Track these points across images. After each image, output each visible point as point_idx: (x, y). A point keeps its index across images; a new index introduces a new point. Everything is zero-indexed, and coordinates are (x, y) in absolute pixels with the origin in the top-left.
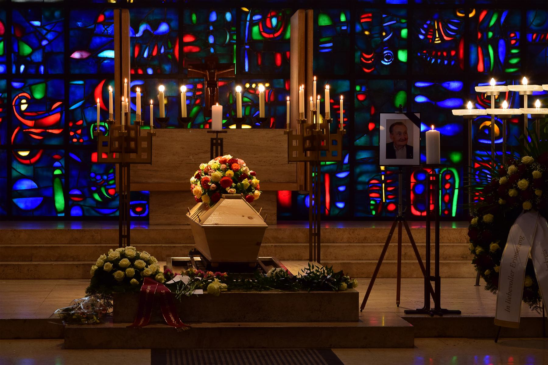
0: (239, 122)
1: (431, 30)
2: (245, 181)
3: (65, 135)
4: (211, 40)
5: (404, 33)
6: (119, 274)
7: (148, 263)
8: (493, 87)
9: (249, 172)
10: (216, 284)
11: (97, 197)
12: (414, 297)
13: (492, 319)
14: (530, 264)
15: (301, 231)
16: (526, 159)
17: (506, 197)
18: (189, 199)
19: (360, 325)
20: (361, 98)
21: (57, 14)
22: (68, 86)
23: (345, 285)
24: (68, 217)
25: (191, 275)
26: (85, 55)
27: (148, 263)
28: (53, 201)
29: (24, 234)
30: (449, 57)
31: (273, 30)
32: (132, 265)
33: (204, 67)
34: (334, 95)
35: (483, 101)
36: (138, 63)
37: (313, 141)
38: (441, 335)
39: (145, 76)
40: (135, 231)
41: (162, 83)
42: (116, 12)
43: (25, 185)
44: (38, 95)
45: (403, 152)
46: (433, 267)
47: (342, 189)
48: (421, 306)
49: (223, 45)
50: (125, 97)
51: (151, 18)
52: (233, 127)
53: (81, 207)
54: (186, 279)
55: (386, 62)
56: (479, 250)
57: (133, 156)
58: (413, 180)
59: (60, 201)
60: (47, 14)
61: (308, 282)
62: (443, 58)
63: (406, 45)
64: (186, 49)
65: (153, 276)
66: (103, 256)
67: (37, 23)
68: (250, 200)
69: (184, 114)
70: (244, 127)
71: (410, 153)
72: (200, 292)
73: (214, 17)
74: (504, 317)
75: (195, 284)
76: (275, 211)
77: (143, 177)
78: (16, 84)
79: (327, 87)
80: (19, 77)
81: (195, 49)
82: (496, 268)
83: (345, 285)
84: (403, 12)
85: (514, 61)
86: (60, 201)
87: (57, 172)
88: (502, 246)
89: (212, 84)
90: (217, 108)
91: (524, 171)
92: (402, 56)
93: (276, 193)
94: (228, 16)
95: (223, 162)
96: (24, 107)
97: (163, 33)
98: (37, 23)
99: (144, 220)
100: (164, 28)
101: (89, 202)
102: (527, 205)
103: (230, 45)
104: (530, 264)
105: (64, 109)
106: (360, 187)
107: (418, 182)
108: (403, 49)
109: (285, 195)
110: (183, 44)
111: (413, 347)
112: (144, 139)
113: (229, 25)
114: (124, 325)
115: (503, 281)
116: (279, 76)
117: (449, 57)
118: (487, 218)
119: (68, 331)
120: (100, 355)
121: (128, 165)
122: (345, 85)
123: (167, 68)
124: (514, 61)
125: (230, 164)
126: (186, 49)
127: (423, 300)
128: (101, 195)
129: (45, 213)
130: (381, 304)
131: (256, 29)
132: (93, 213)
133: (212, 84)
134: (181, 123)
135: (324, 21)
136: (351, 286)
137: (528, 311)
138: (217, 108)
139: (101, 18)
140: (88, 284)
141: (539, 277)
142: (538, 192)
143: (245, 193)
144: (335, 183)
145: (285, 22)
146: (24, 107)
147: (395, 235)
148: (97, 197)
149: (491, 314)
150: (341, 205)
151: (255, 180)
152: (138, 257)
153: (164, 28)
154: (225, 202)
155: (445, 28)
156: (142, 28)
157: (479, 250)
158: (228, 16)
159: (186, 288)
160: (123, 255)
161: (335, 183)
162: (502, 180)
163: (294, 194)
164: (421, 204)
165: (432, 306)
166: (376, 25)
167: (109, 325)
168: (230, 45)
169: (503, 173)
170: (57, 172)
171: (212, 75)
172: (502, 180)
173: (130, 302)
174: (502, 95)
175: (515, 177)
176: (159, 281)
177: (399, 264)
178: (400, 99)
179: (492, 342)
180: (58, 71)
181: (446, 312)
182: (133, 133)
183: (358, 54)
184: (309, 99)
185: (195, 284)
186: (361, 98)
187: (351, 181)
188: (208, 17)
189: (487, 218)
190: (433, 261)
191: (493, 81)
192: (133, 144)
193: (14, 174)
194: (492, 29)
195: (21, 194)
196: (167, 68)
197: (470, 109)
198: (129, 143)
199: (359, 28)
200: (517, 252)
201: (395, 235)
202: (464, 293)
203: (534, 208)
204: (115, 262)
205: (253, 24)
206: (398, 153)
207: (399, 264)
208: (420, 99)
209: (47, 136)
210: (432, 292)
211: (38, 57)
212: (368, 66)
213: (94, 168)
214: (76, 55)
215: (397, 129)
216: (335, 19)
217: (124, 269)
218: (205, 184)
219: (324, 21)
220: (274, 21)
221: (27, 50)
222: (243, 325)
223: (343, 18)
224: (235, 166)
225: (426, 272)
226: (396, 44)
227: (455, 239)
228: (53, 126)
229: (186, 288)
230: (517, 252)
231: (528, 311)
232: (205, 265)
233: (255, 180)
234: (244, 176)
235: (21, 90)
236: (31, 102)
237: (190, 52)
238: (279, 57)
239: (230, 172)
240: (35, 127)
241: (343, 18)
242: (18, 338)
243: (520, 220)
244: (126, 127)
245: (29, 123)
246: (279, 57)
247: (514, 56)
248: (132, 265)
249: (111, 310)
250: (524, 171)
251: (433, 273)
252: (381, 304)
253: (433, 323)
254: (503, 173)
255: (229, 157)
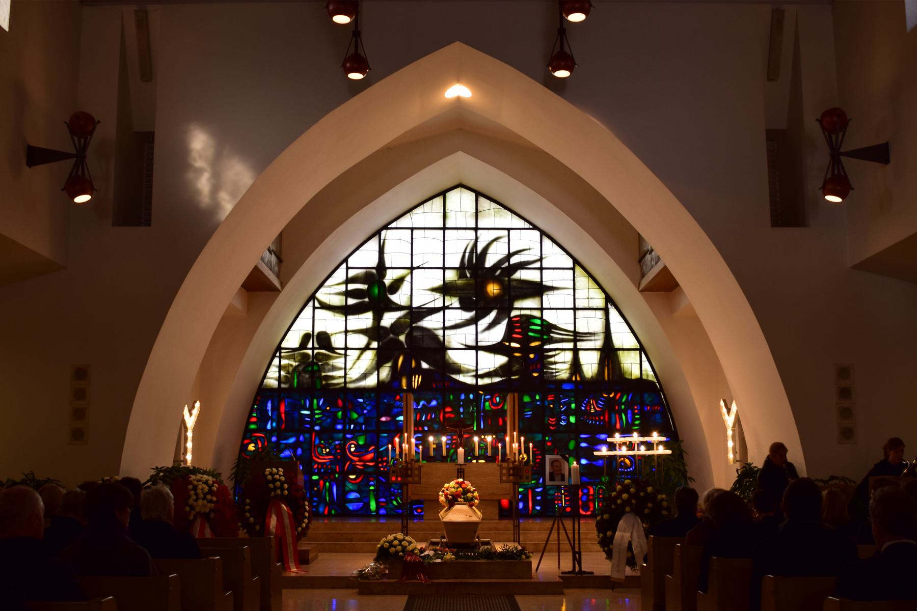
0: (478, 458)
1: (588, 404)
2: (469, 495)
3: (376, 466)
4: (461, 410)
5: (573, 406)
6: (392, 550)
7: (410, 543)
8: (617, 438)
9: (473, 489)
10: (449, 556)
11: (395, 503)
12: (567, 564)
13: (609, 577)
14: (630, 543)
15: (508, 524)
16: (627, 481)
17: (616, 504)
18: (440, 506)
19: (532, 580)
20: (549, 444)
21: (373, 395)
22: (378, 437)
23: (524, 557)
24: (378, 515)
25: (435, 550)
26: (389, 419)
27: (410, 543)
28: (369, 506)
29: (351, 525)
30: (600, 421)
31: (498, 404)
32: (400, 544)
33: (456, 426)
34: (526, 442)
35: (612, 447)
36: (418, 424)
37: (517, 472)
38: (582, 587)
39: (423, 431)
40: (412, 524)
41: (432, 435)
42: (404, 394)
43: (353, 496)
44: (361, 443)
45: (558, 477)
46: (577, 546)
47: (539, 498)
48: (571, 569)
49: (468, 413)
50: (408, 444)
51: (427, 397)
52: (474, 461)
53: (385, 509)
54: (431, 553)
55: (563, 423)
56: (601, 535)
57: (410, 479)
58: (580, 493)
59: (373, 506)
60: (367, 395)
61: (505, 555)
62: (596, 421)
63: (575, 413)
64: (447, 415)
65: (412, 551)
66: (384, 539)
67: (361, 400)
68: (471, 506)
69: (444, 453)
70: (480, 461)
71: (563, 479)
72: (439, 561)
73: (463, 397)
74: (616, 576)
75: (437, 556)
76: (497, 511)
77: (414, 491)
78: (348, 436)
79: (522, 439)
80: (350, 431)
81: (452, 416)
82: (611, 546)
83: (524, 557)
84: (572, 394)
85: (637, 422)
86: (373, 506)
87: (372, 488)
88: (614, 533)
89: (461, 436)
90: (461, 450)
91: (626, 489)
92: (572, 419)
93: (499, 502)
94: (471, 396)
95: (457, 483)
96: (353, 449)
97: (434, 406)
98: (361, 400)
99: (420, 517)
100: (434, 403)
101: (390, 506)
102: (627, 509)
103: (473, 413)
104: (630, 543)
105: (376, 451)
106: (549, 497)
107: (584, 494)
108: (572, 415)
109: (505, 502)
110: (445, 413)
111: (563, 594)
112: (416, 469)
113: (472, 401)
114: (393, 581)
115: (615, 555)
116: (500, 432)
117: (600, 421)
118: (606, 516)
119: (362, 585)
120: (378, 598)
121: (407, 484)
122: (539, 437)
123: (436, 426)
124: (637, 422)
125: (460, 484)
126: (447, 415)
127: (571, 565)
128: (397, 502)
129: (364, 512)
130: (547, 567)
131: (487, 404)
132: (393, 513)
133: (461, 436)
134: (444, 459)
135: (527, 399)
136: (528, 557)
137: (628, 571)
138: (461, 450)
139: (398, 397)
140: (375, 555)
141: (635, 552)
142: (633, 501)
143: (469, 502)
144: (535, 494)
145: (503, 400)
146: (353, 449)
147: (556, 526)
148: (395, 503)
149: (608, 574)
150: (538, 508)
151: (476, 494)
152: (404, 540)
153: (434, 403)
154: (457, 507)
155: (597, 403)
156: (422, 403)
157: (601, 535)
158: (471, 396)
159: (431, 558)
160: (395, 539)
161: (535, 494)
162: (614, 494)
163: (510, 502)
164: (586, 508)
165: (577, 569)
166: (557, 401)
167: (385, 580)
168: (473, 413)
169: (614, 490)
170: (372, 488)
171: (461, 431)
172: (614, 494)
173: (399, 569)
174: (642, 443)
175: (620, 493)
176: (416, 554)
177: (559, 544)
178: (572, 445)
179: (610, 591)
180: (373, 428)
181: (585, 572)
182: (409, 466)
183: (546, 418)
184: (514, 443)
185: (437, 556)
186: (549, 444)
187: (544, 493)
188: (460, 396)
189: (606, 516)
190: (577, 542)
191: (635, 434)
192: (409, 472)
193: (347, 489)
194: (624, 403)
195: (351, 501)
196: (436, 426)
197: (604, 451)
198: (408, 469)
199: (546, 403)
200: (622, 537)
201: (556, 526)
202: (596, 562)
203: (632, 510)
204: (391, 543)
205: (485, 400)
206: (556, 478)
207: (559, 544)
208: (583, 445)
209: (365, 466)
210: (577, 560)
211: (361, 420)
212: (552, 425)
213: (393, 486)
214: (383, 419)
215: (556, 464)
216: (533, 398)
217: (395, 547)
218: (446, 496)
219: (527, 399)
220: (498, 399)
221: (355, 416)
222: (463, 581)
223: (537, 398)
224: (463, 485)
225: (573, 548)
226: (569, 412)
227: (589, 529)
228: (370, 461)
229: (431, 558)
230: (622, 537)
231: (628, 571)
232: (446, 545)
233: (476, 494)
234: (469, 491)
235: (351, 439)
236: (357, 446)
237: (449, 417)
238: (501, 420)
239: (460, 489)
240: (359, 461)
241: (537, 398)
242: (333, 588)
243: (624, 517)
244: (406, 461)
245: (356, 459)
246: (501, 420)
247: (637, 419)
248: (400, 544)
249: (387, 572)
250: (626, 489)
251: (577, 550)
252: (547, 567)
253: (577, 580)
254: (614, 490)
255: (461, 480)
